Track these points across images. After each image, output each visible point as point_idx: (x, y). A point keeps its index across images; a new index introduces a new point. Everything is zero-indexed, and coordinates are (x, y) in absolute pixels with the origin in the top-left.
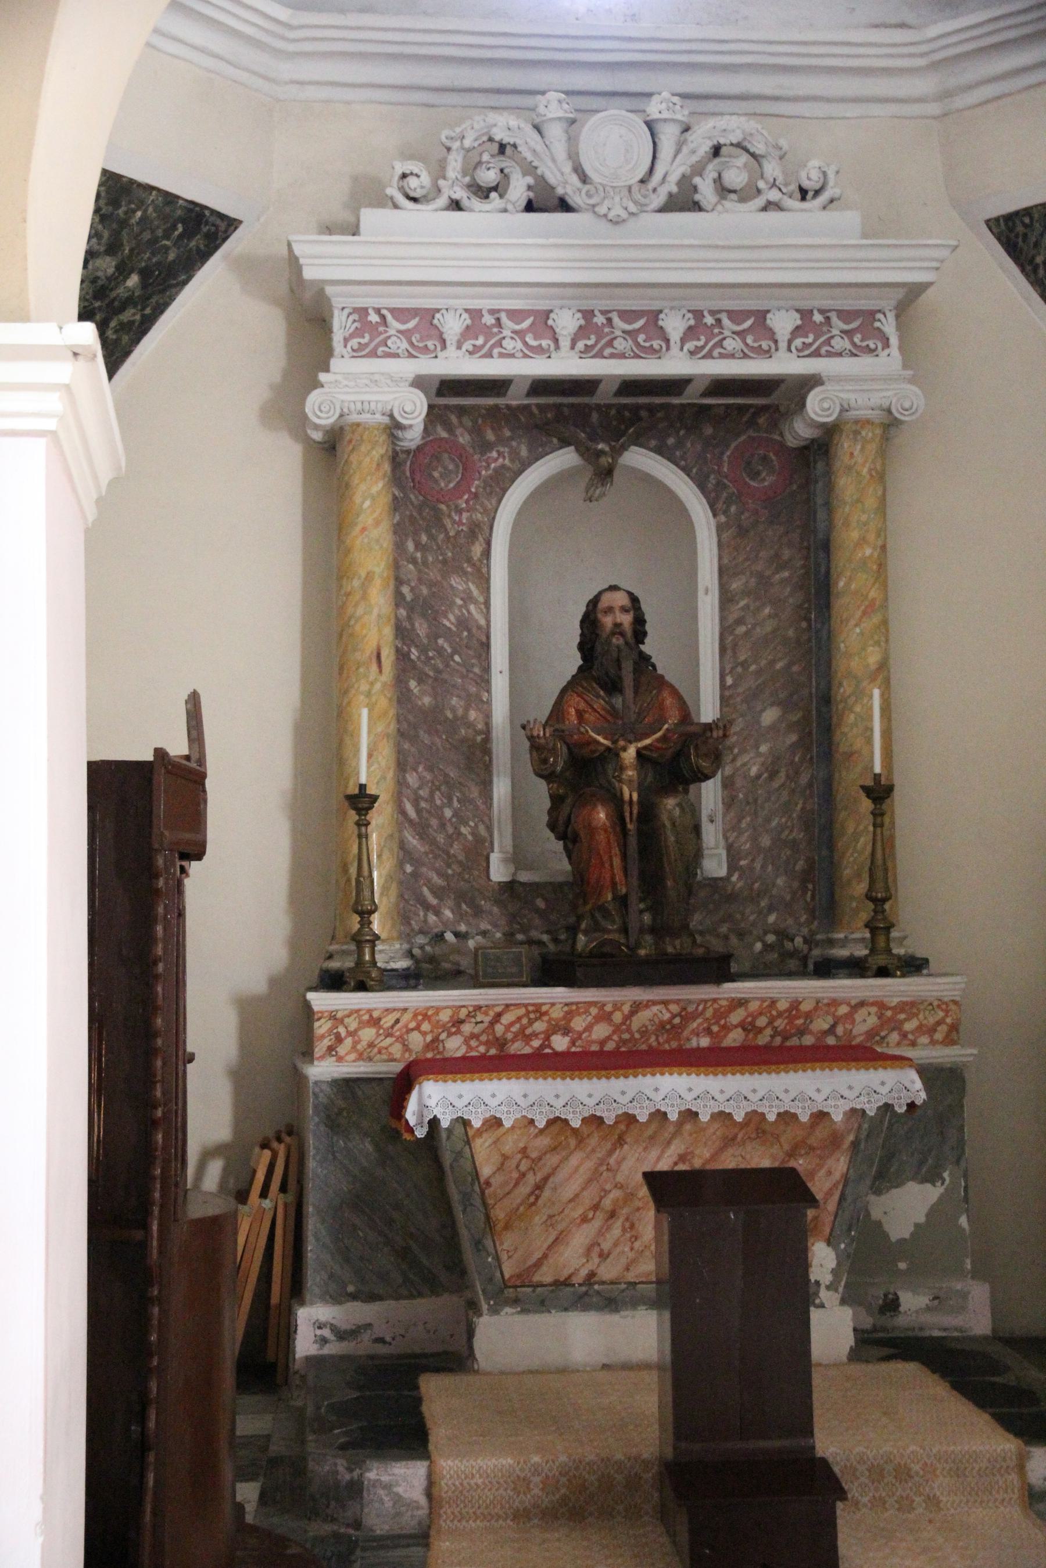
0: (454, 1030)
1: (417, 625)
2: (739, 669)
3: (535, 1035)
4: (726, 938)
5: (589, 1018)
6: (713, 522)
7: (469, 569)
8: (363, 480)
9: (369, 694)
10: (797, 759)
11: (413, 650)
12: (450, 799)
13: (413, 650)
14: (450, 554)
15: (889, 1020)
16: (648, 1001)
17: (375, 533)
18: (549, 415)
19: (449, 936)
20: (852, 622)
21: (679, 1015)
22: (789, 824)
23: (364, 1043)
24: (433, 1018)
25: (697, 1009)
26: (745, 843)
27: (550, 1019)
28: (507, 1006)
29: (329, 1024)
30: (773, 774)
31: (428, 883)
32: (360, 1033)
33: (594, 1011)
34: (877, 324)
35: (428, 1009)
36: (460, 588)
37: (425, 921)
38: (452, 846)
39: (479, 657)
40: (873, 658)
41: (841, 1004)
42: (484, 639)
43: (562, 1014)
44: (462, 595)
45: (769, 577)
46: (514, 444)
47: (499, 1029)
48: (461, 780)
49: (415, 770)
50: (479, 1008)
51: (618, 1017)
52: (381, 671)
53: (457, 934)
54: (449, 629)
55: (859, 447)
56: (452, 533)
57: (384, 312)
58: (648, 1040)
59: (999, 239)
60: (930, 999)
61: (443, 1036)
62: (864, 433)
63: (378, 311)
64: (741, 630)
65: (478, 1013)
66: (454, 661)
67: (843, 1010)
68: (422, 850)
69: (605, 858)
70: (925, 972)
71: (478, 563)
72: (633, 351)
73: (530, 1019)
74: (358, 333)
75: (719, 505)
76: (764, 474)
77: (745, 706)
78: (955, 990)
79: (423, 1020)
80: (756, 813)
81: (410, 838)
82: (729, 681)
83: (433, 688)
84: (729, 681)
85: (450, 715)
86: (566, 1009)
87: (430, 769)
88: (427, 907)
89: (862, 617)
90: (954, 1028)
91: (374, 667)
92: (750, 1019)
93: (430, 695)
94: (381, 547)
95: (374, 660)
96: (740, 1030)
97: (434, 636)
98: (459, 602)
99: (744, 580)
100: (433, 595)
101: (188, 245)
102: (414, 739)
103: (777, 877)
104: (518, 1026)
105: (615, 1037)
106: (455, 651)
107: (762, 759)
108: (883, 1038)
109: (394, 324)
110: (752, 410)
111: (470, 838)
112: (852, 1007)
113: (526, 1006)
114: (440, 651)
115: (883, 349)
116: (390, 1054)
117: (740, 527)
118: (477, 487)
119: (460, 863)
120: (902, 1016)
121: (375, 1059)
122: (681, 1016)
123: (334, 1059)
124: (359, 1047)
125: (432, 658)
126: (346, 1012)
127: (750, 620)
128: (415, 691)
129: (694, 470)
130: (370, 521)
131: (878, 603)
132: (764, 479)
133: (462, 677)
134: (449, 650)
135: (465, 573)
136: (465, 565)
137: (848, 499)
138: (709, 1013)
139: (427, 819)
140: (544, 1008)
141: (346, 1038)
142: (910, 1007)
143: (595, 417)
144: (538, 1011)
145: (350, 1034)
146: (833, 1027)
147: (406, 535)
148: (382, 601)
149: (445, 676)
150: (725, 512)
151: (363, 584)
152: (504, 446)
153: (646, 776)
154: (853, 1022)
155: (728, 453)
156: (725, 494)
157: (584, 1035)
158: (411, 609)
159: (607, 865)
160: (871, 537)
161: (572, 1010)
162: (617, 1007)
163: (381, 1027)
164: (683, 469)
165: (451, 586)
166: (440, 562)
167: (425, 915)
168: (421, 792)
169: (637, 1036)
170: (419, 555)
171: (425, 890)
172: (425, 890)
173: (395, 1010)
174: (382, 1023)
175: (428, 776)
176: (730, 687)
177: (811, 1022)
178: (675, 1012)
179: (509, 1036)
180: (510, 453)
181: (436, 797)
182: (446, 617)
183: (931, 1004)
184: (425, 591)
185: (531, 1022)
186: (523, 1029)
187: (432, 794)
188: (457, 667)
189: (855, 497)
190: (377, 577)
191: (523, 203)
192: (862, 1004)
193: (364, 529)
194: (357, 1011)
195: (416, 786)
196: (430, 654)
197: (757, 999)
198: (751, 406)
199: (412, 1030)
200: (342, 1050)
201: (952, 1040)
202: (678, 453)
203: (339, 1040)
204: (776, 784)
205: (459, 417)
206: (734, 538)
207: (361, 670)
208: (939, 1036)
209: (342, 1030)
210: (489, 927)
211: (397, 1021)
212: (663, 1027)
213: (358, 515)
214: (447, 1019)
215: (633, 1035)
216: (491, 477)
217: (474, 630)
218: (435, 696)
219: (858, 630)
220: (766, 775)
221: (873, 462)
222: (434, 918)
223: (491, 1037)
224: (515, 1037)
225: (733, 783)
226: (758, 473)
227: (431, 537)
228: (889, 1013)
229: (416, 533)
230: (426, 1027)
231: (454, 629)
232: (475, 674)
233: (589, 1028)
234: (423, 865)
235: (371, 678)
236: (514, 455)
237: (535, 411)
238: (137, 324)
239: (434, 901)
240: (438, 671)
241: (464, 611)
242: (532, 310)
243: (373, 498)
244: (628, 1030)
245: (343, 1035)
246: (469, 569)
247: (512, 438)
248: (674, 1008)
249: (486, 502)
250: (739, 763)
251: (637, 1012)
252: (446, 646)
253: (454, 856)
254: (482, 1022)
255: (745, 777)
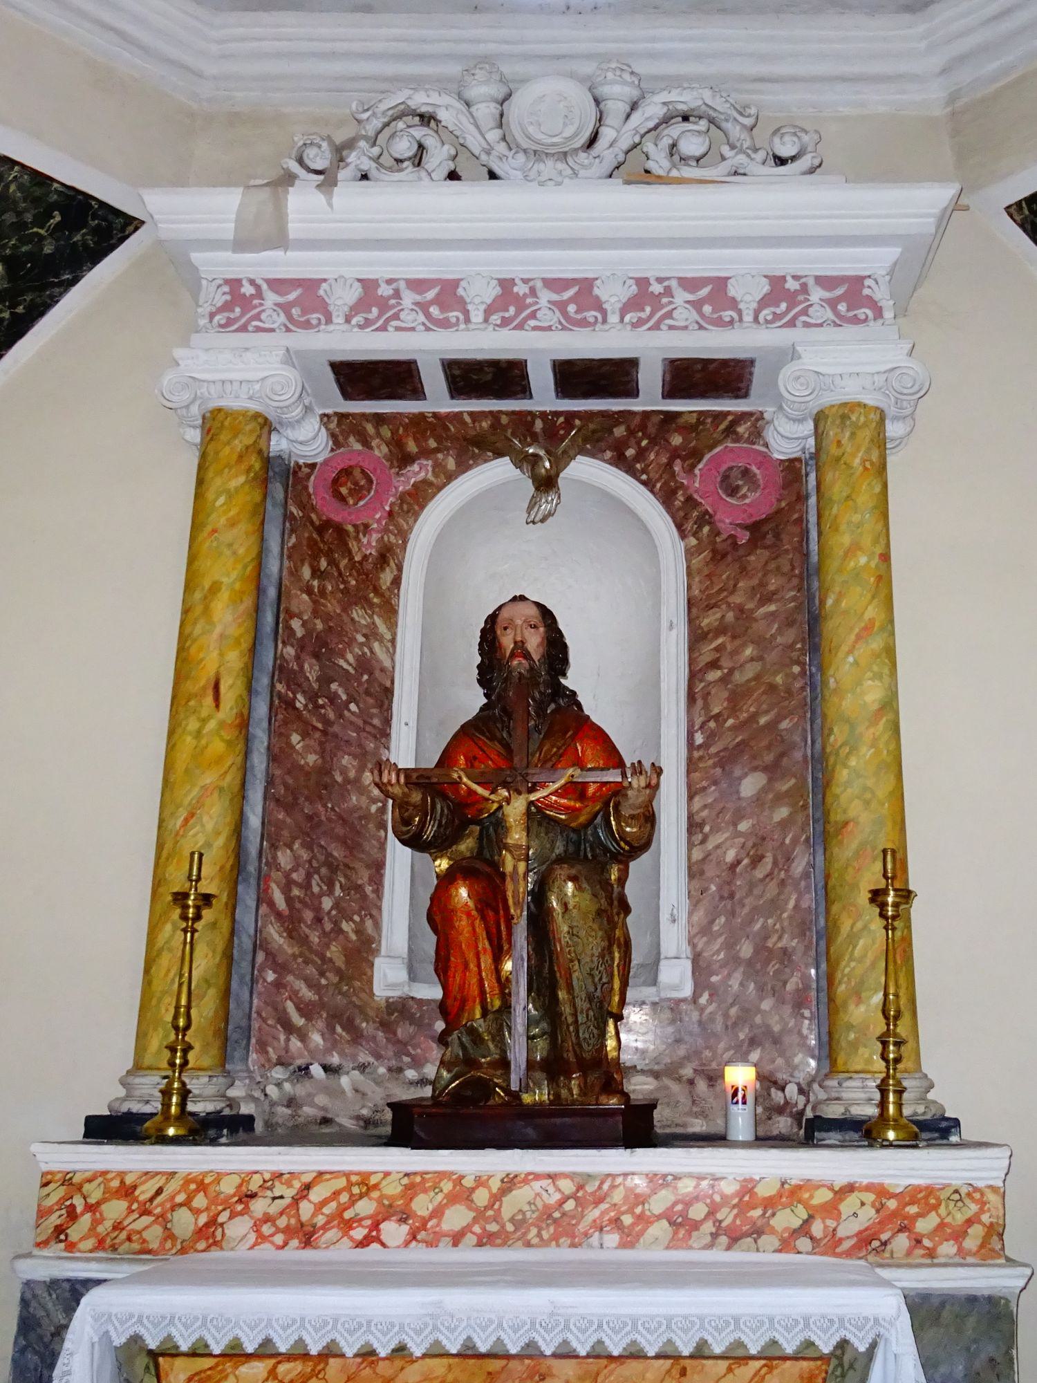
0: (240, 1207)
1: (306, 666)
2: (712, 724)
3: (358, 1220)
4: (691, 1082)
5: (440, 1197)
6: (680, 546)
7: (375, 600)
8: (219, 473)
9: (198, 734)
10: (787, 841)
11: (299, 696)
12: (331, 885)
13: (299, 696)
14: (353, 582)
15: (895, 1214)
16: (529, 1174)
17: (227, 536)
18: (484, 424)
19: (316, 1070)
20: (845, 648)
21: (573, 1196)
22: (778, 926)
23: (108, 1224)
24: (212, 1189)
25: (600, 1187)
26: (718, 952)
27: (382, 1197)
28: (321, 1174)
29: (61, 1192)
30: (757, 860)
31: (295, 996)
32: (104, 1207)
33: (447, 1186)
34: (866, 292)
35: (205, 1174)
36: (363, 622)
37: (287, 1050)
38: (328, 948)
39: (381, 706)
40: (873, 694)
41: (818, 1187)
42: (388, 684)
43: (400, 1189)
44: (364, 631)
45: (752, 611)
46: (440, 456)
47: (306, 1209)
48: (346, 860)
49: (290, 847)
50: (278, 1176)
51: (481, 1197)
52: (217, 706)
53: (327, 1068)
54: (347, 671)
55: (847, 434)
56: (357, 558)
57: (259, 282)
58: (525, 1234)
59: (1022, 226)
60: (956, 1183)
61: (223, 1218)
62: (854, 418)
63: (252, 282)
64: (714, 675)
65: (277, 1183)
66: (349, 710)
67: (822, 1196)
68: (290, 951)
69: (471, 956)
70: (954, 1139)
71: (387, 594)
72: (560, 323)
73: (352, 1195)
74: (227, 307)
75: (689, 525)
76: (744, 490)
77: (718, 770)
78: (992, 1169)
79: (197, 1191)
80: (733, 913)
81: (276, 936)
82: (699, 739)
83: (321, 744)
84: (699, 739)
85: (339, 779)
86: (405, 1181)
87: (308, 846)
88: (289, 1028)
89: (856, 642)
90: (996, 1231)
91: (209, 700)
92: (679, 1207)
93: (315, 752)
94: (234, 553)
95: (210, 693)
96: (665, 1223)
97: (325, 680)
98: (361, 639)
99: (718, 616)
100: (330, 629)
101: (70, 237)
102: (289, 808)
103: (762, 999)
104: (333, 1205)
105: (477, 1229)
106: (351, 699)
107: (742, 840)
108: (885, 1244)
109: (271, 298)
110: (730, 418)
111: (354, 937)
112: (836, 1193)
113: (347, 1175)
114: (333, 698)
115: (875, 319)
116: (144, 1241)
117: (714, 551)
118: (391, 506)
119: (338, 972)
120: (913, 1210)
121: (121, 1249)
122: (577, 1199)
123: (62, 1245)
124: (100, 1229)
125: (323, 707)
126: (88, 1175)
127: (726, 663)
128: (298, 747)
129: (658, 485)
130: (223, 520)
131: (877, 624)
132: (744, 496)
133: (359, 730)
134: (344, 697)
135: (371, 605)
136: (372, 595)
137: (835, 498)
138: (617, 1196)
139: (299, 911)
140: (373, 1180)
141: (82, 1214)
142: (925, 1197)
143: (539, 424)
144: (365, 1184)
145: (90, 1208)
146: (807, 1222)
147: (302, 562)
148: (229, 617)
149: (336, 729)
150: (694, 535)
151: (206, 598)
152: (427, 459)
153: (553, 843)
154: (838, 1217)
155: (700, 466)
156: (695, 514)
157: (430, 1224)
158: (301, 646)
159: (472, 966)
160: (867, 541)
161: (414, 1184)
162: (480, 1182)
163: (136, 1200)
164: (644, 483)
165: (352, 619)
166: (342, 591)
167: (288, 1040)
168: (294, 876)
169: (510, 1227)
170: (315, 583)
171: (290, 1006)
172: (290, 1006)
173: (157, 1174)
174: (137, 1193)
175: (305, 855)
176: (700, 747)
177: (773, 1215)
178: (567, 1192)
179: (320, 1220)
180: (434, 467)
181: (314, 883)
182: (343, 657)
183: (956, 1191)
184: (319, 625)
185: (353, 1201)
186: (343, 1209)
187: (309, 876)
188: (353, 718)
189: (845, 494)
190: (224, 588)
191: (446, 173)
192: (850, 1188)
193: (214, 531)
194: (104, 1173)
195: (288, 867)
196: (320, 702)
197: (690, 1175)
198: (729, 413)
199: (181, 1205)
200: (74, 1233)
201: (993, 1250)
202: (638, 466)
203: (72, 1215)
204: (759, 873)
205: (377, 427)
206: (707, 564)
207: (192, 703)
208: (971, 1243)
209: (78, 1202)
210: (371, 1060)
211: (159, 1191)
212: (550, 1216)
213: (209, 515)
214: (232, 1191)
215: (503, 1226)
216: (409, 493)
217: (377, 673)
218: (322, 753)
219: (851, 659)
220: (746, 861)
221: (868, 451)
222: (299, 1044)
223: (293, 1221)
224: (328, 1222)
225: (702, 873)
226: (738, 488)
227: (332, 563)
228: (892, 1204)
229: (315, 558)
230: (200, 1201)
231: (353, 672)
232: (374, 726)
233: (438, 1213)
234: (290, 972)
235: (204, 714)
236: (438, 468)
237: (467, 419)
238: (6, 323)
239: (299, 1021)
240: (327, 722)
241: (366, 650)
242: (440, 280)
243: (230, 497)
244: (496, 1218)
245: (79, 1209)
246: (375, 600)
247: (437, 450)
248: (567, 1186)
249: (401, 521)
250: (710, 845)
251: (510, 1190)
252: (341, 692)
253: (331, 960)
254: (281, 1197)
255: (718, 863)
